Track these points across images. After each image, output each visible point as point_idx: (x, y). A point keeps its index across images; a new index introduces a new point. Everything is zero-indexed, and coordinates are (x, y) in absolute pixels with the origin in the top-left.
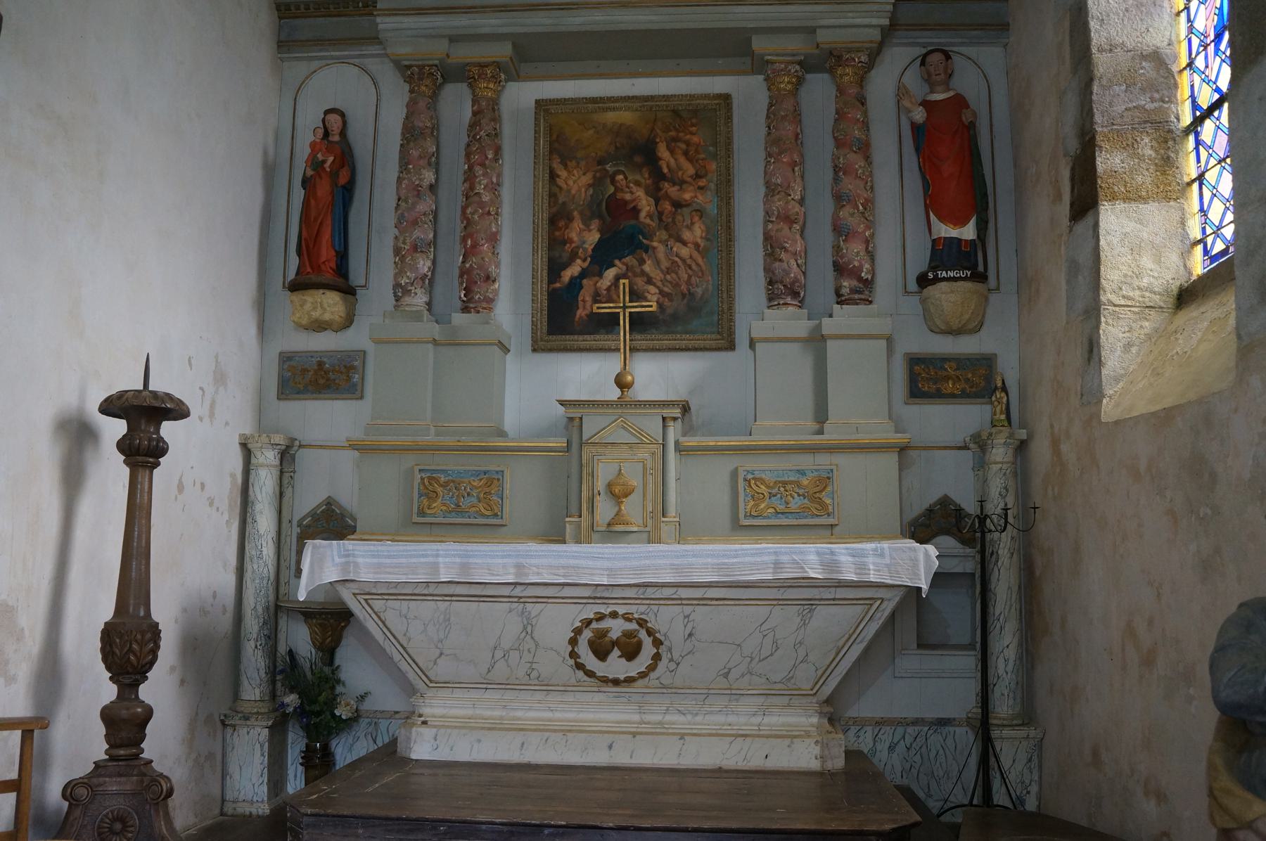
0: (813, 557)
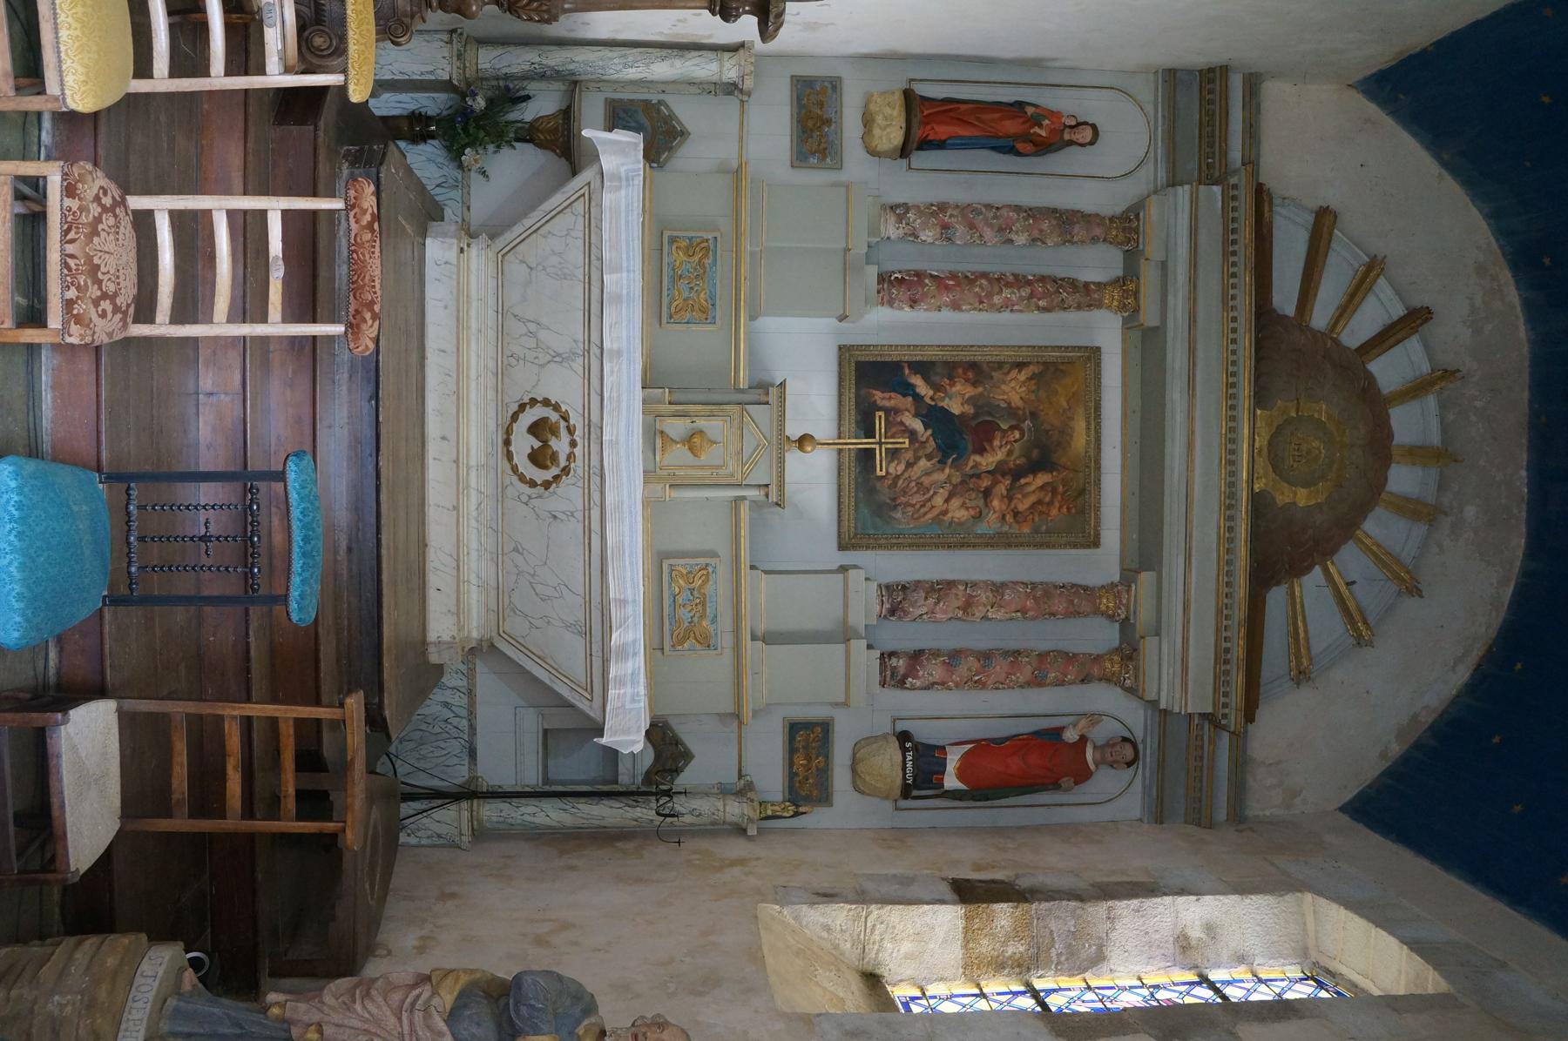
0: (630, 637)
